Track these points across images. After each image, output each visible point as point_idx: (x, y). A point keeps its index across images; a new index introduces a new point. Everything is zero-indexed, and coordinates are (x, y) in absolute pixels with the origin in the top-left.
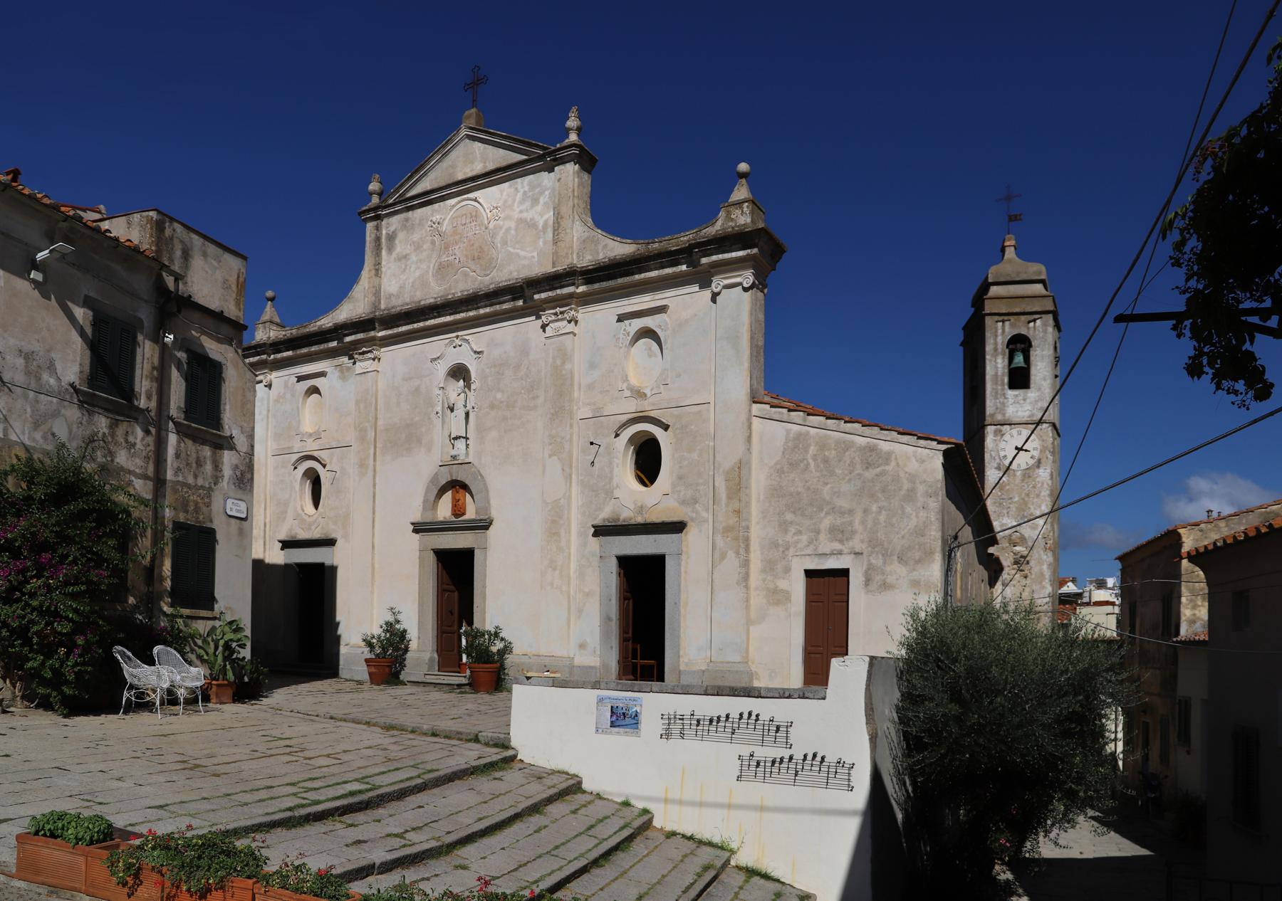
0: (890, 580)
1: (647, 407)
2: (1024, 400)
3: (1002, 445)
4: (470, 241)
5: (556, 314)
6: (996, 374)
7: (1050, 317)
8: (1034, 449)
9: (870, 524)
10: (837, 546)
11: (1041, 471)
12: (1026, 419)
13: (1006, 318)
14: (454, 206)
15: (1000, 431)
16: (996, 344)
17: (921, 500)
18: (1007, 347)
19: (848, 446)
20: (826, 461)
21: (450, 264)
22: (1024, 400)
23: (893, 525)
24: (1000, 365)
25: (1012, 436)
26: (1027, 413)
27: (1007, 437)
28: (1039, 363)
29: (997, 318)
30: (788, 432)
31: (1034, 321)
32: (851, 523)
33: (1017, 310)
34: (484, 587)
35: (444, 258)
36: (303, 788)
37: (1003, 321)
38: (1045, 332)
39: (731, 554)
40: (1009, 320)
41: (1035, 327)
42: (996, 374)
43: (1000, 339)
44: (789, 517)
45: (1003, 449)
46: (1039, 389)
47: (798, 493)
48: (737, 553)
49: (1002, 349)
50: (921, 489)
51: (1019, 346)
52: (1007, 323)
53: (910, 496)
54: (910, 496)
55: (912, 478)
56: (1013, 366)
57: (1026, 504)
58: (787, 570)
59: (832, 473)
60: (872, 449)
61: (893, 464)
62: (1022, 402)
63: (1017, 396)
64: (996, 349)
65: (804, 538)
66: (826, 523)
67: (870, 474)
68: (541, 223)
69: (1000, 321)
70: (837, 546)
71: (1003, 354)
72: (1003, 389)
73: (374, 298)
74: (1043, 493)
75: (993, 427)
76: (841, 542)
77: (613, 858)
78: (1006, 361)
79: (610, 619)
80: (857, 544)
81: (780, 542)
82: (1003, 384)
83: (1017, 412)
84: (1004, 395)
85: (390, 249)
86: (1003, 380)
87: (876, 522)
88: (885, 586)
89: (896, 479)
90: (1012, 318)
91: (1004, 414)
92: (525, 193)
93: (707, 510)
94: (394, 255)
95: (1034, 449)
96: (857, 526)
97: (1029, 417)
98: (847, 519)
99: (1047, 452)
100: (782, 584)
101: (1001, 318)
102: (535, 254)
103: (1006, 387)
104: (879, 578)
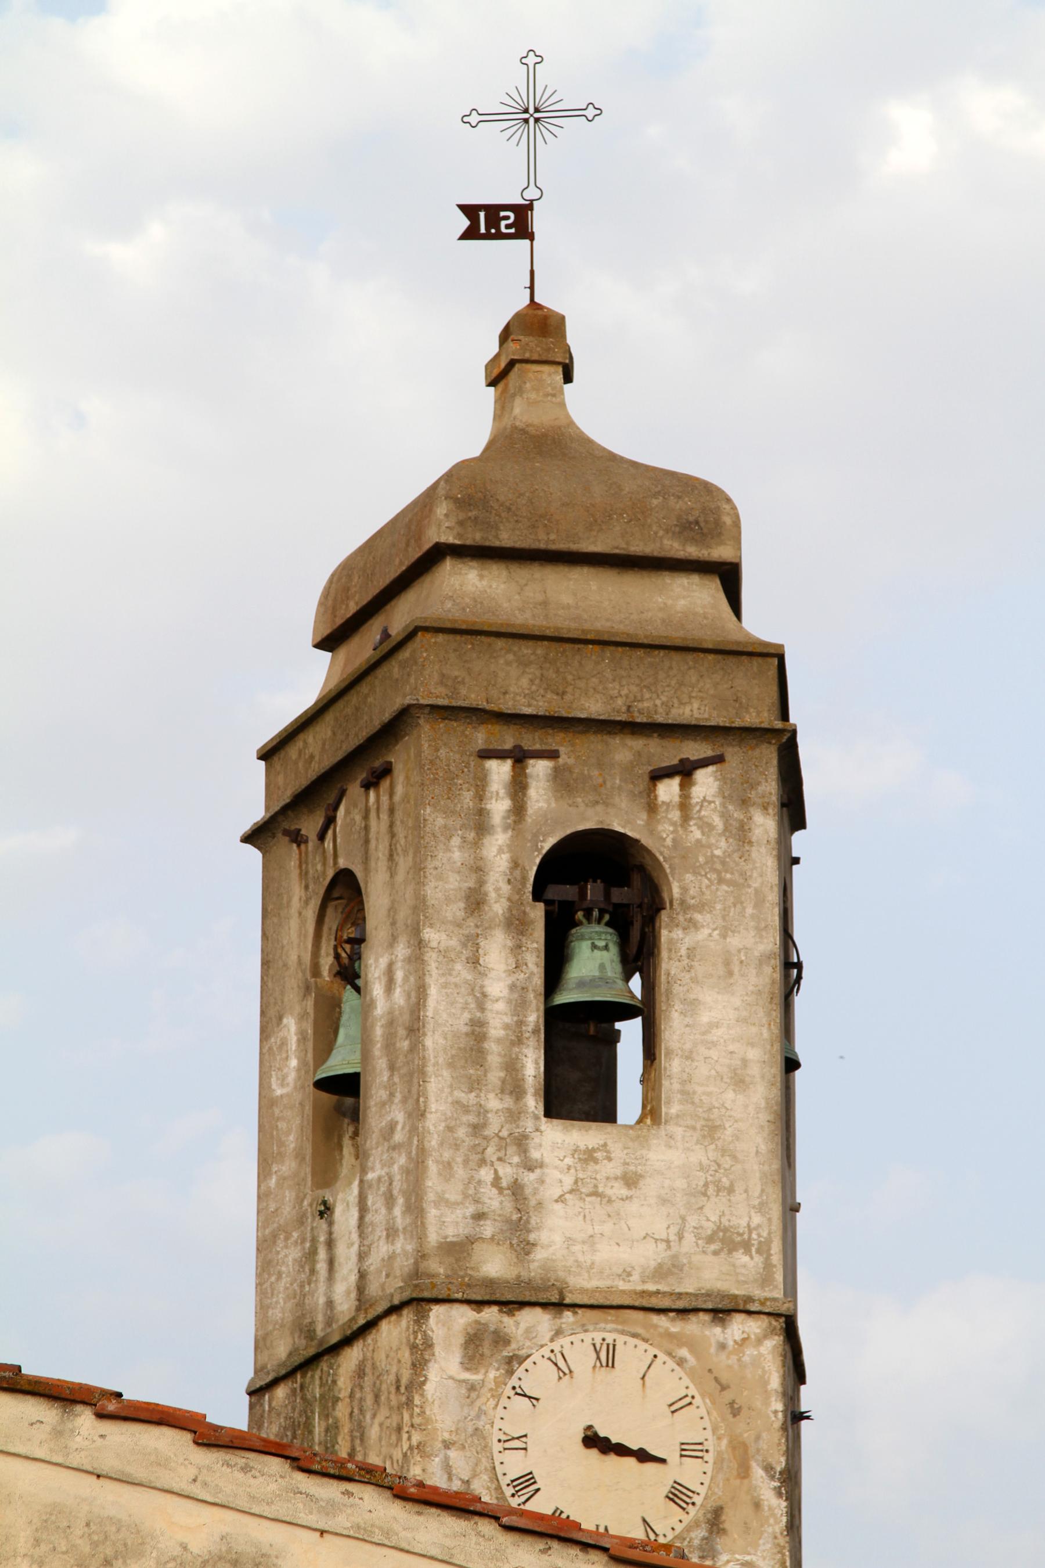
2: (631, 1180)
6: (477, 1032)
7: (560, 369)
8: (686, 1451)
12: (635, 1284)
13: (531, 740)
15: (501, 1339)
18: (537, 895)
22: (631, 1180)
24: (497, 987)
25: (565, 1372)
26: (649, 1255)
28: (707, 996)
29: (480, 737)
31: (685, 771)
36: (601, 1348)
37: (519, 757)
38: (741, 834)
40: (553, 755)
41: (684, 805)
42: (477, 1032)
45: (518, 1442)
49: (515, 904)
52: (539, 769)
56: (564, 997)
62: (618, 1190)
63: (588, 1157)
69: (500, 755)
71: (516, 924)
72: (514, 1116)
75: (462, 1317)
77: (591, 1551)
82: (514, 1088)
83: (591, 1240)
84: (521, 1142)
86: (512, 1067)
91: (525, 1248)
95: (686, 1451)
97: (660, 1272)
99: (758, 1472)
101: (508, 739)
103: (533, 1103)
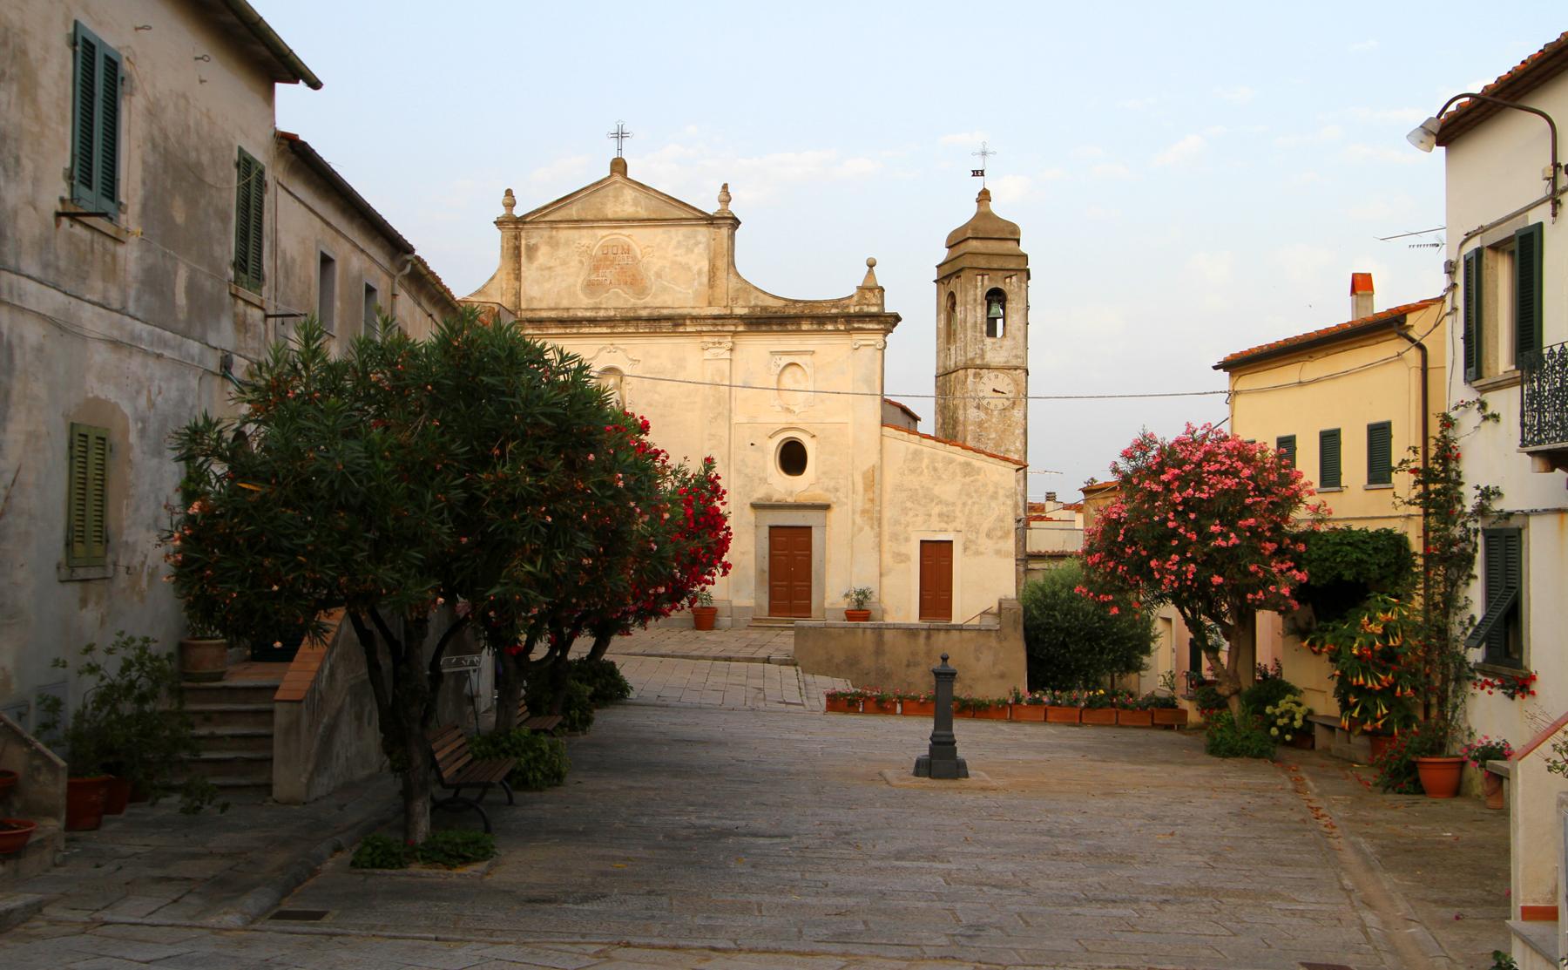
0: (982, 549)
1: (792, 419)
3: (981, 386)
4: (622, 268)
5: (714, 343)
6: (976, 323)
8: (1010, 392)
9: (967, 511)
10: (943, 525)
11: (1015, 412)
13: (985, 272)
14: (603, 237)
16: (976, 295)
17: (1001, 499)
19: (951, 461)
20: (935, 469)
21: (600, 284)
23: (982, 514)
24: (979, 315)
26: (1003, 360)
27: (985, 380)
29: (976, 272)
30: (907, 448)
31: (1011, 277)
32: (954, 511)
33: (995, 266)
34: (1529, 653)
35: (593, 277)
37: (983, 275)
39: (867, 528)
42: (976, 323)
43: (979, 291)
44: (909, 505)
45: (982, 391)
46: (1014, 339)
47: (916, 490)
48: (872, 528)
50: (1001, 492)
51: (995, 298)
53: (994, 496)
54: (994, 496)
55: (996, 485)
57: (1001, 439)
58: (907, 540)
59: (940, 478)
60: (968, 464)
61: (982, 474)
64: (975, 300)
65: (920, 519)
66: (936, 510)
67: (968, 480)
68: (695, 269)
70: (943, 525)
71: (982, 304)
72: (982, 337)
73: (513, 298)
74: (1017, 431)
75: (973, 370)
76: (947, 523)
78: (985, 311)
79: (764, 571)
80: (957, 525)
81: (903, 521)
82: (982, 332)
84: (983, 341)
85: (530, 258)
86: (981, 329)
87: (971, 512)
88: (978, 553)
89: (985, 485)
90: (991, 274)
92: (679, 242)
93: (847, 497)
94: (536, 264)
96: (958, 514)
98: (951, 508)
100: (903, 549)
102: (690, 291)
103: (985, 334)
104: (973, 547)
